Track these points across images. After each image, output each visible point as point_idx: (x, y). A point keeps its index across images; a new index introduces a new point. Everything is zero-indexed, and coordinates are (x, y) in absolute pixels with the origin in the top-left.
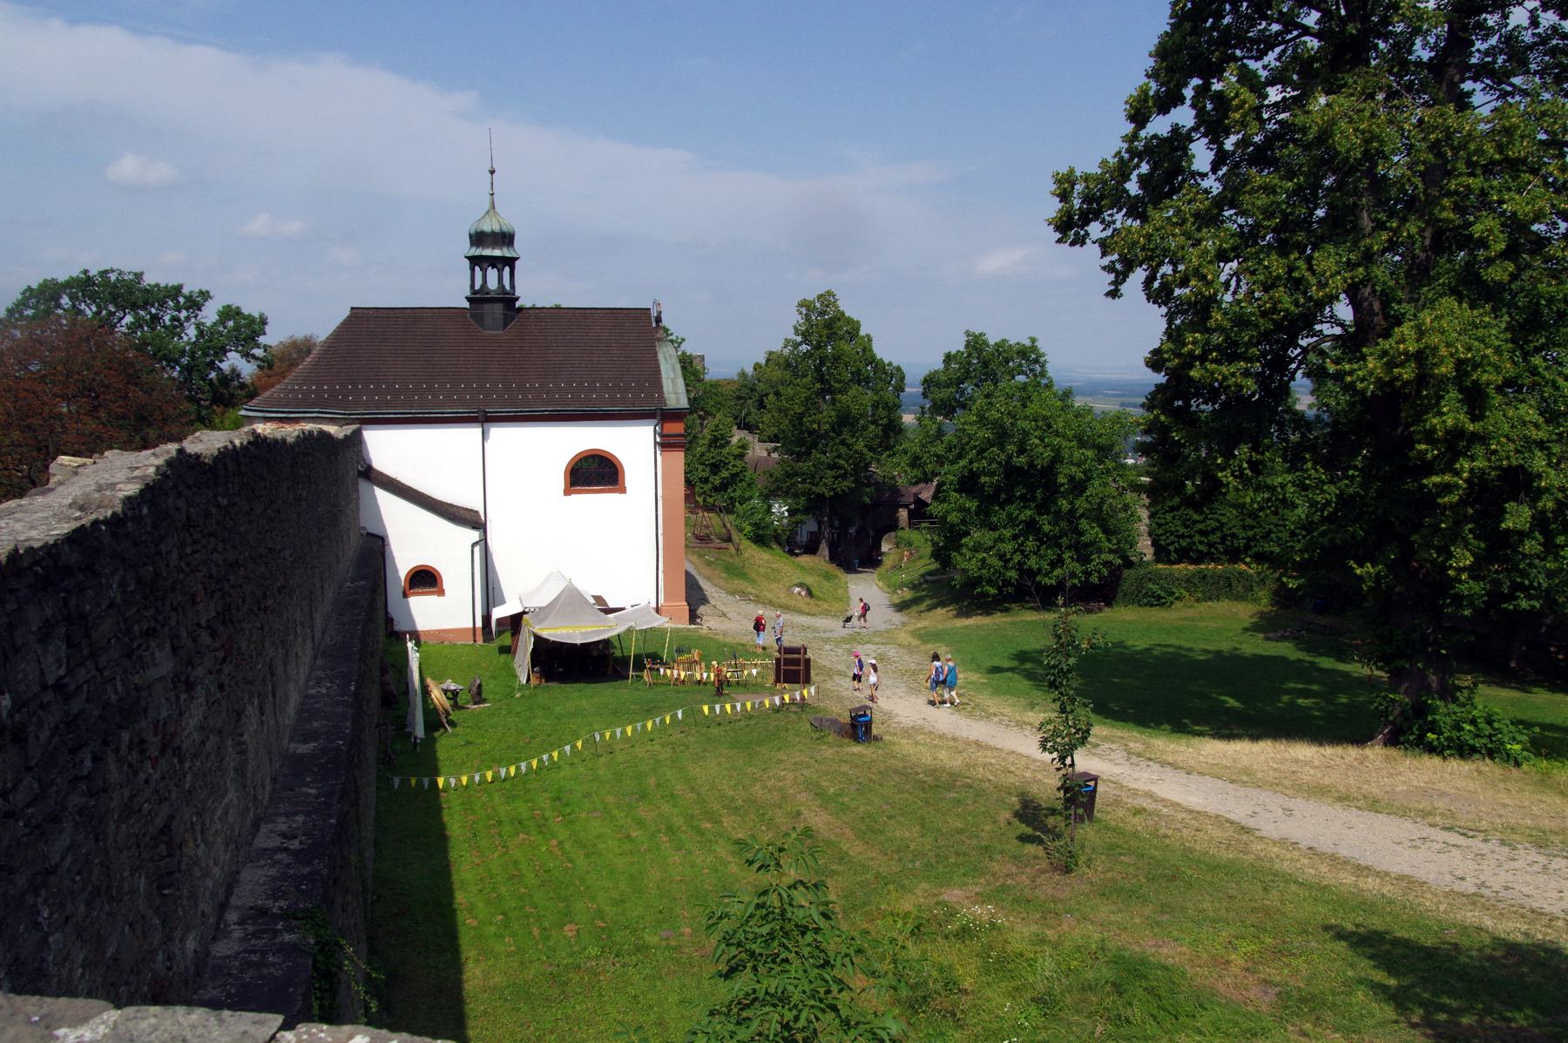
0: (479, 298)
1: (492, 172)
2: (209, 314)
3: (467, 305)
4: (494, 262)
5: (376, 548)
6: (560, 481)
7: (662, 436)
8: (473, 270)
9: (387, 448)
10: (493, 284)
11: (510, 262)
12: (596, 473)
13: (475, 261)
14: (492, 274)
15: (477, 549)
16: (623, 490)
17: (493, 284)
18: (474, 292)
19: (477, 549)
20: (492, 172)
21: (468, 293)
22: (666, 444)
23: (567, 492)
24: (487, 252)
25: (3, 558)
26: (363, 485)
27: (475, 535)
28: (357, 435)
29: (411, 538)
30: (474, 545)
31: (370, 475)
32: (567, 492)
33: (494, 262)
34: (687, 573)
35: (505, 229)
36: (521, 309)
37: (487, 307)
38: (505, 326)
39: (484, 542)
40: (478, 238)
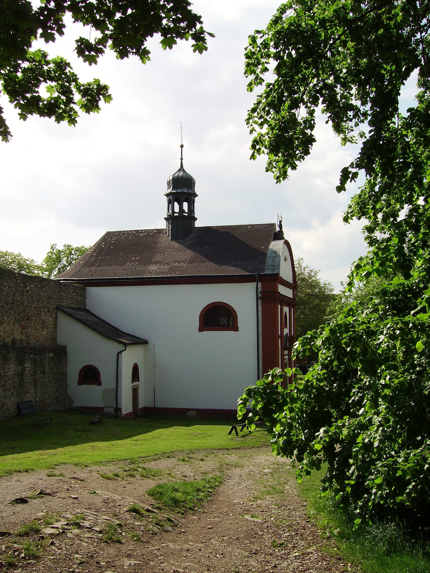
1: (182, 146)
5: (61, 352)
12: (217, 318)
20: (182, 146)
32: (201, 329)
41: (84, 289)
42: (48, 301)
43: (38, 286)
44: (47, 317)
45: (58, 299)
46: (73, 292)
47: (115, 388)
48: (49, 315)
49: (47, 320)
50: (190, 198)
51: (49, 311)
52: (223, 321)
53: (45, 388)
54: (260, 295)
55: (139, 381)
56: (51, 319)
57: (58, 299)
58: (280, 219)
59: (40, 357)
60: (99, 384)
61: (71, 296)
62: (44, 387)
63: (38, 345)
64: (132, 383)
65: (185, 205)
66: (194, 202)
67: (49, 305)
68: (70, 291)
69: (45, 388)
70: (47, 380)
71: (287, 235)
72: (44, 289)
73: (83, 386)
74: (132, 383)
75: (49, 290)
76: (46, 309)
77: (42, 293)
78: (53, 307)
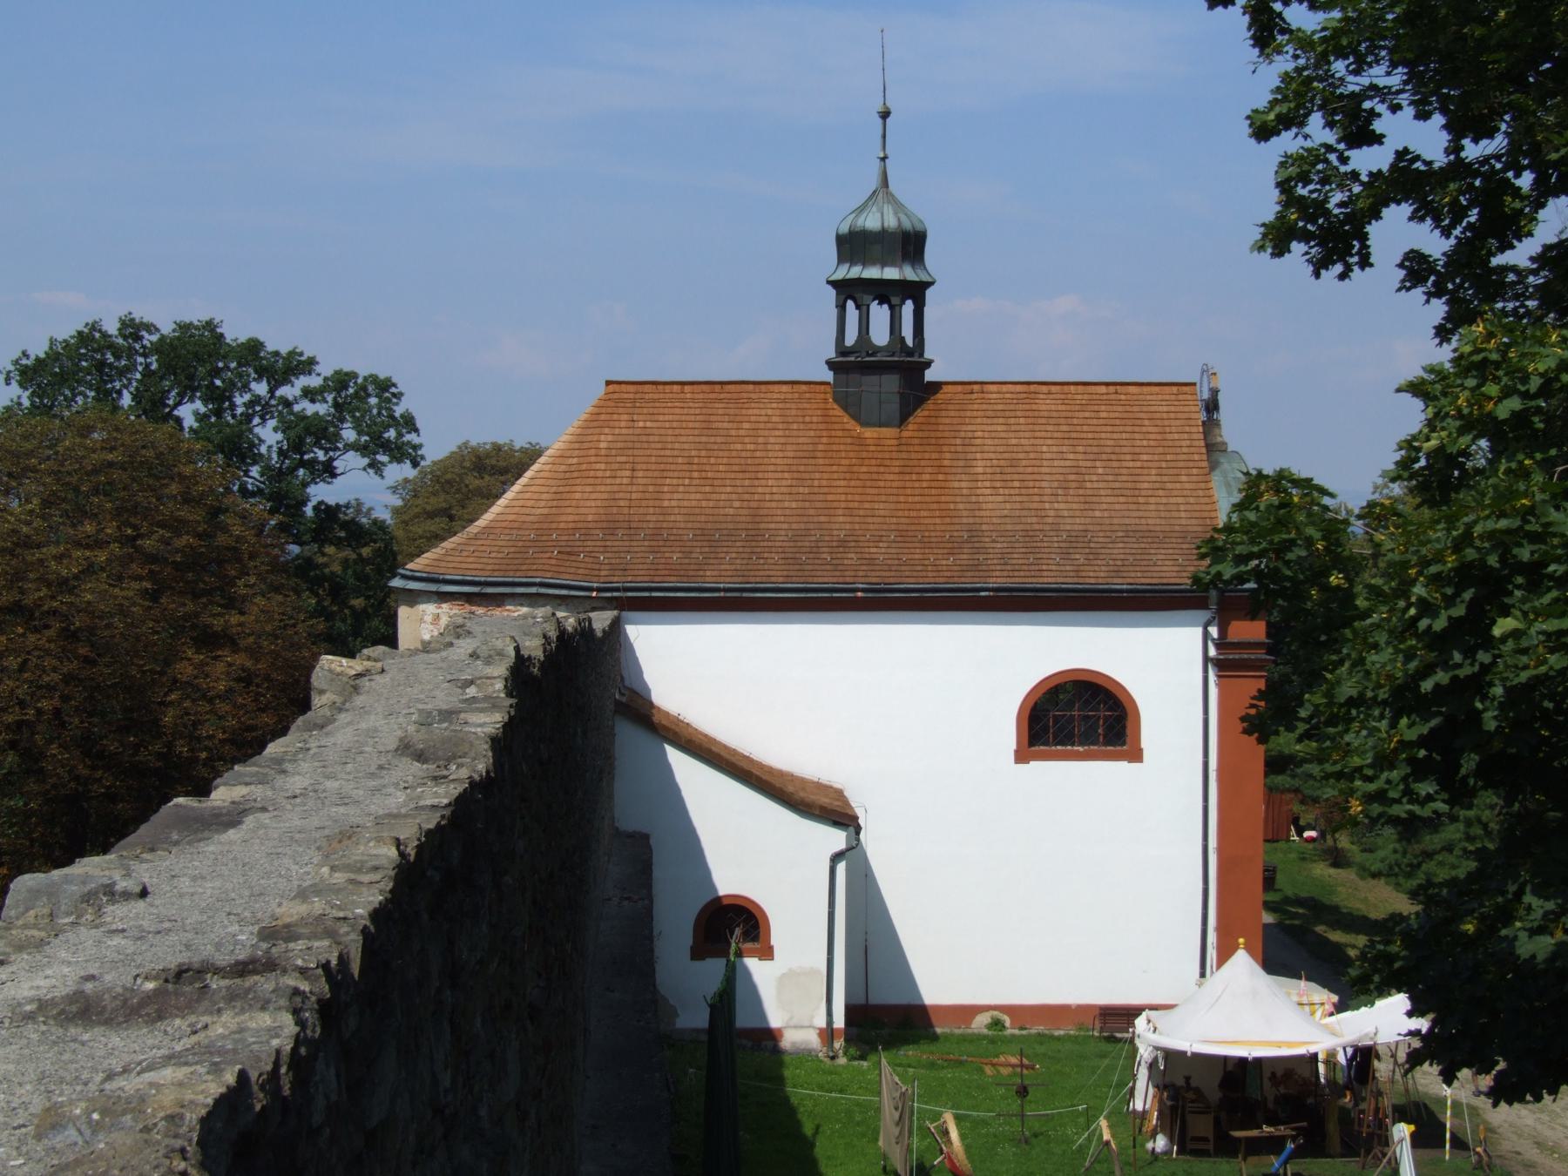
0: (852, 364)
1: (885, 115)
2: (411, 437)
3: (829, 376)
4: (885, 292)
6: (1007, 733)
7: (1218, 646)
8: (842, 308)
9: (677, 661)
10: (880, 335)
11: (916, 291)
12: (1079, 718)
13: (846, 290)
14: (880, 315)
15: (841, 867)
16: (1136, 755)
17: (880, 335)
18: (842, 350)
19: (841, 867)
21: (831, 353)
23: (1021, 757)
24: (873, 273)
25: (1564, 1088)
26: (628, 736)
27: (837, 839)
28: (616, 628)
29: (742, 846)
30: (836, 858)
31: (640, 711)
32: (1021, 757)
33: (885, 292)
34: (533, 454)
35: (907, 225)
36: (936, 387)
37: (871, 381)
38: (903, 419)
39: (852, 857)
40: (853, 245)
54: (1212, 652)
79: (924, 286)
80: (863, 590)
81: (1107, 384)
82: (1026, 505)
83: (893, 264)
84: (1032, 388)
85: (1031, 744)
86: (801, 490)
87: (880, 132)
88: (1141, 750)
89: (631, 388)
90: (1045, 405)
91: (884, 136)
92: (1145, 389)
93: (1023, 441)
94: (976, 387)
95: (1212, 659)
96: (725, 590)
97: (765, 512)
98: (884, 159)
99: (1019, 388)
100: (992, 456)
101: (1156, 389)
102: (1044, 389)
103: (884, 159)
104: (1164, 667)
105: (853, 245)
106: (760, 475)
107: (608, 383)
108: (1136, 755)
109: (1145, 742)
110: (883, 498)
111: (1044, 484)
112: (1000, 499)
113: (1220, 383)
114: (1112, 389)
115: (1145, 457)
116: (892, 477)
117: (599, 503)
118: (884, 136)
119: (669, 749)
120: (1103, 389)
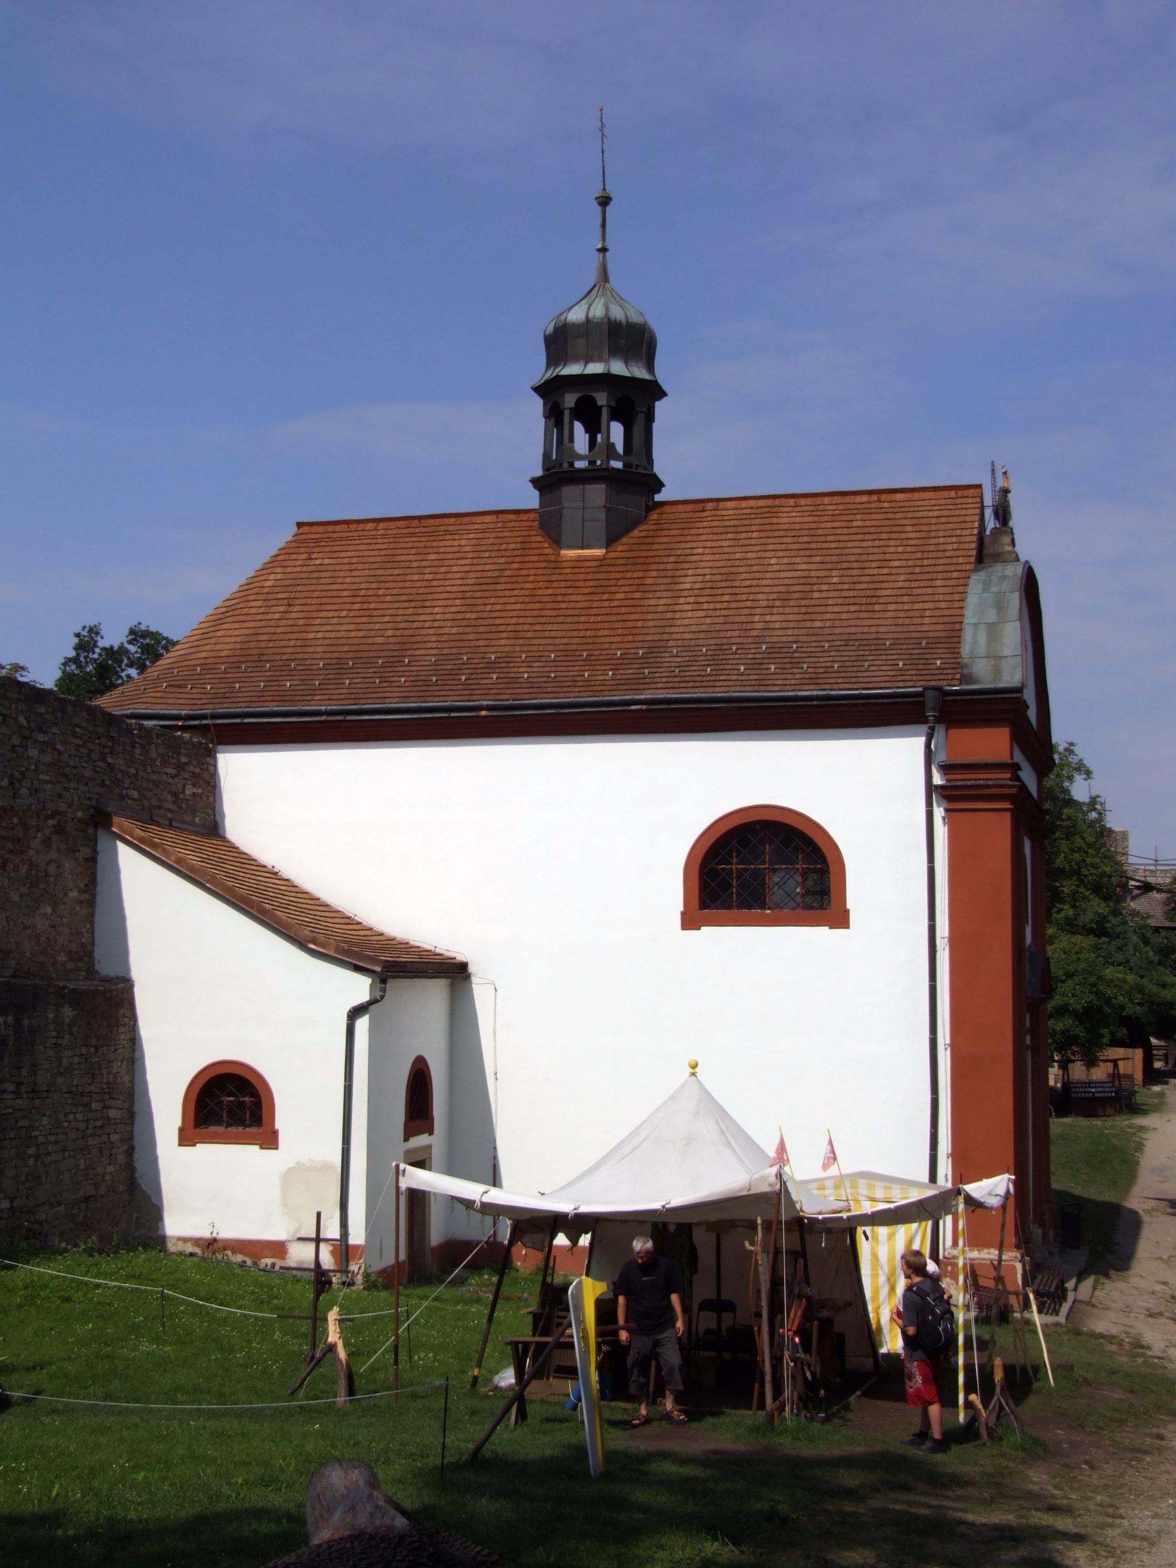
1: (604, 201)
3: (531, 499)
5: (105, 1008)
6: (671, 890)
7: (945, 768)
12: (761, 871)
22: (955, 790)
23: (690, 921)
30: (356, 1013)
32: (690, 921)
40: (560, 343)
41: (211, 754)
42: (59, 787)
43: (16, 720)
44: (53, 855)
45: (103, 784)
46: (165, 762)
47: (807, 1236)
48: (63, 846)
49: (52, 870)
50: (636, 402)
51: (60, 830)
52: (786, 881)
53: (37, 1157)
54: (938, 780)
55: (431, 1132)
56: (68, 865)
57: (103, 784)
58: (1000, 483)
59: (18, 1022)
60: (270, 1140)
61: (155, 777)
62: (31, 1151)
63: (9, 972)
64: (406, 1139)
65: (617, 432)
66: (650, 417)
67: (63, 807)
68: (153, 754)
69: (37, 1157)
70: (45, 1121)
71: (1031, 540)
72: (41, 737)
73: (201, 1148)
74: (406, 1139)
75: (64, 743)
76: (50, 822)
77: (33, 752)
78: (80, 814)
79: (655, 391)
80: (488, 708)
81: (870, 493)
82: (731, 619)
83: (599, 359)
84: (777, 502)
85: (703, 905)
86: (468, 616)
87: (599, 221)
88: (847, 912)
89: (321, 529)
90: (788, 517)
91: (603, 226)
92: (916, 495)
93: (749, 555)
94: (710, 505)
95: (937, 787)
96: (328, 713)
97: (419, 639)
98: (603, 250)
99: (761, 503)
100: (707, 571)
101: (931, 495)
102: (792, 502)
103: (603, 250)
104: (870, 795)
105: (560, 343)
106: (428, 603)
107: (300, 525)
108: (841, 920)
109: (853, 901)
110: (560, 619)
111: (760, 597)
112: (701, 614)
113: (1012, 485)
114: (875, 497)
115: (896, 564)
116: (579, 598)
117: (239, 639)
118: (603, 226)
119: (122, 848)
120: (865, 498)
